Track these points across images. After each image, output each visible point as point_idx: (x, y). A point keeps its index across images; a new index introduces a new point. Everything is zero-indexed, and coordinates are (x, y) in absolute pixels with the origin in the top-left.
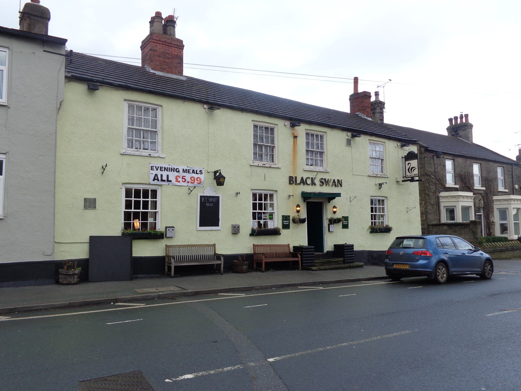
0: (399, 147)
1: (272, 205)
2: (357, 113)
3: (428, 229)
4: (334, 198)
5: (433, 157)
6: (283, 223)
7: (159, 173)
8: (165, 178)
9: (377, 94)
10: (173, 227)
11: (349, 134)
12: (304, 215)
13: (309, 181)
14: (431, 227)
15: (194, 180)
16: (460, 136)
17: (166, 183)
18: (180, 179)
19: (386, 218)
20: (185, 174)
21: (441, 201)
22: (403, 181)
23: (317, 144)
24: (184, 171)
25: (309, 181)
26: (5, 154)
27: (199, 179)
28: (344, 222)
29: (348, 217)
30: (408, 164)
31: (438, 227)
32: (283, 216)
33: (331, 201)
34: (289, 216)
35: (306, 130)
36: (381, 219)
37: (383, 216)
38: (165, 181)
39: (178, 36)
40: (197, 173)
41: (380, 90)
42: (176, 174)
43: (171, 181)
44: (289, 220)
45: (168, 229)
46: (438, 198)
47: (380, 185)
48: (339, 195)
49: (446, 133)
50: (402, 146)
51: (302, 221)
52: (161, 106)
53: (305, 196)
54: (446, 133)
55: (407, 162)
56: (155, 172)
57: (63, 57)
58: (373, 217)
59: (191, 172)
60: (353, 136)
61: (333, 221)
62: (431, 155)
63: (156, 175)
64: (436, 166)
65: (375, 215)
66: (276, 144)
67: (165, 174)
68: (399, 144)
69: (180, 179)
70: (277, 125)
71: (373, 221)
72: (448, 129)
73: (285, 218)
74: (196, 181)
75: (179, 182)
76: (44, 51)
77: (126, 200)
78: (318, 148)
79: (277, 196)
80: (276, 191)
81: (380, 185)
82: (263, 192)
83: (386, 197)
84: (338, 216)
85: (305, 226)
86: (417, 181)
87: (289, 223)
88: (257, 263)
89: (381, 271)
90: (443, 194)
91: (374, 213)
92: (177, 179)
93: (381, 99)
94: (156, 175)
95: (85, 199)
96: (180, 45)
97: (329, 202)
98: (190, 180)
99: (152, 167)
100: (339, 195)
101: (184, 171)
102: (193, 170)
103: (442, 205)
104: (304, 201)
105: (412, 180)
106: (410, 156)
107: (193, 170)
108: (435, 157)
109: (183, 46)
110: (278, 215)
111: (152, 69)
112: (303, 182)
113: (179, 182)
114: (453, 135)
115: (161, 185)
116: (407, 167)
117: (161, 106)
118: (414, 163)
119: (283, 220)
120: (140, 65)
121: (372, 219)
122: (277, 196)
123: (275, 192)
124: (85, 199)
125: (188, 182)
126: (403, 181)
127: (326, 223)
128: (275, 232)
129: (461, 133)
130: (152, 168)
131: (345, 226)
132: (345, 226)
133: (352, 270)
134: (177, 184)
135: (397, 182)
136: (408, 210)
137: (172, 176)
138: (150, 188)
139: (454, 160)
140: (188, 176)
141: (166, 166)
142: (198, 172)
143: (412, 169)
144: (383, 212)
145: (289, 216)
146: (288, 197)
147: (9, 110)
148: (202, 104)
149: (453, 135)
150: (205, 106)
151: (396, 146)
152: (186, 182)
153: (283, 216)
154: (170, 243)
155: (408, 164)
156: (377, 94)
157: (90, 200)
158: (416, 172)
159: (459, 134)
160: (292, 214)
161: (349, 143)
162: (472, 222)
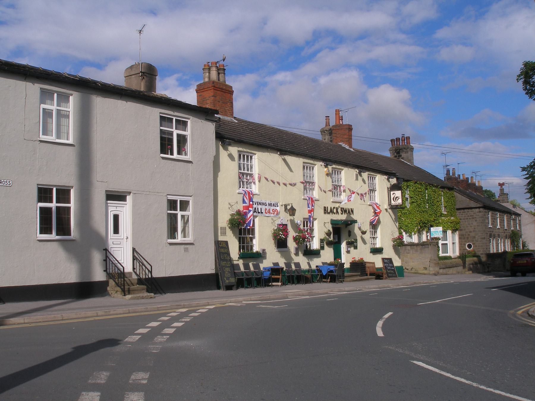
13: (335, 211)
16: (403, 158)
17: (260, 215)
23: (247, 165)
24: (270, 205)
25: (335, 211)
35: (304, 163)
55: (392, 193)
67: (260, 207)
73: (322, 241)
78: (248, 170)
88: (272, 274)
89: (374, 277)
101: (270, 205)
109: (233, 92)
112: (332, 211)
114: (396, 157)
116: (392, 197)
129: (403, 155)
131: (184, 205)
137: (264, 207)
143: (396, 198)
147: (302, 180)
149: (396, 157)
159: (401, 156)
162: (424, 242)
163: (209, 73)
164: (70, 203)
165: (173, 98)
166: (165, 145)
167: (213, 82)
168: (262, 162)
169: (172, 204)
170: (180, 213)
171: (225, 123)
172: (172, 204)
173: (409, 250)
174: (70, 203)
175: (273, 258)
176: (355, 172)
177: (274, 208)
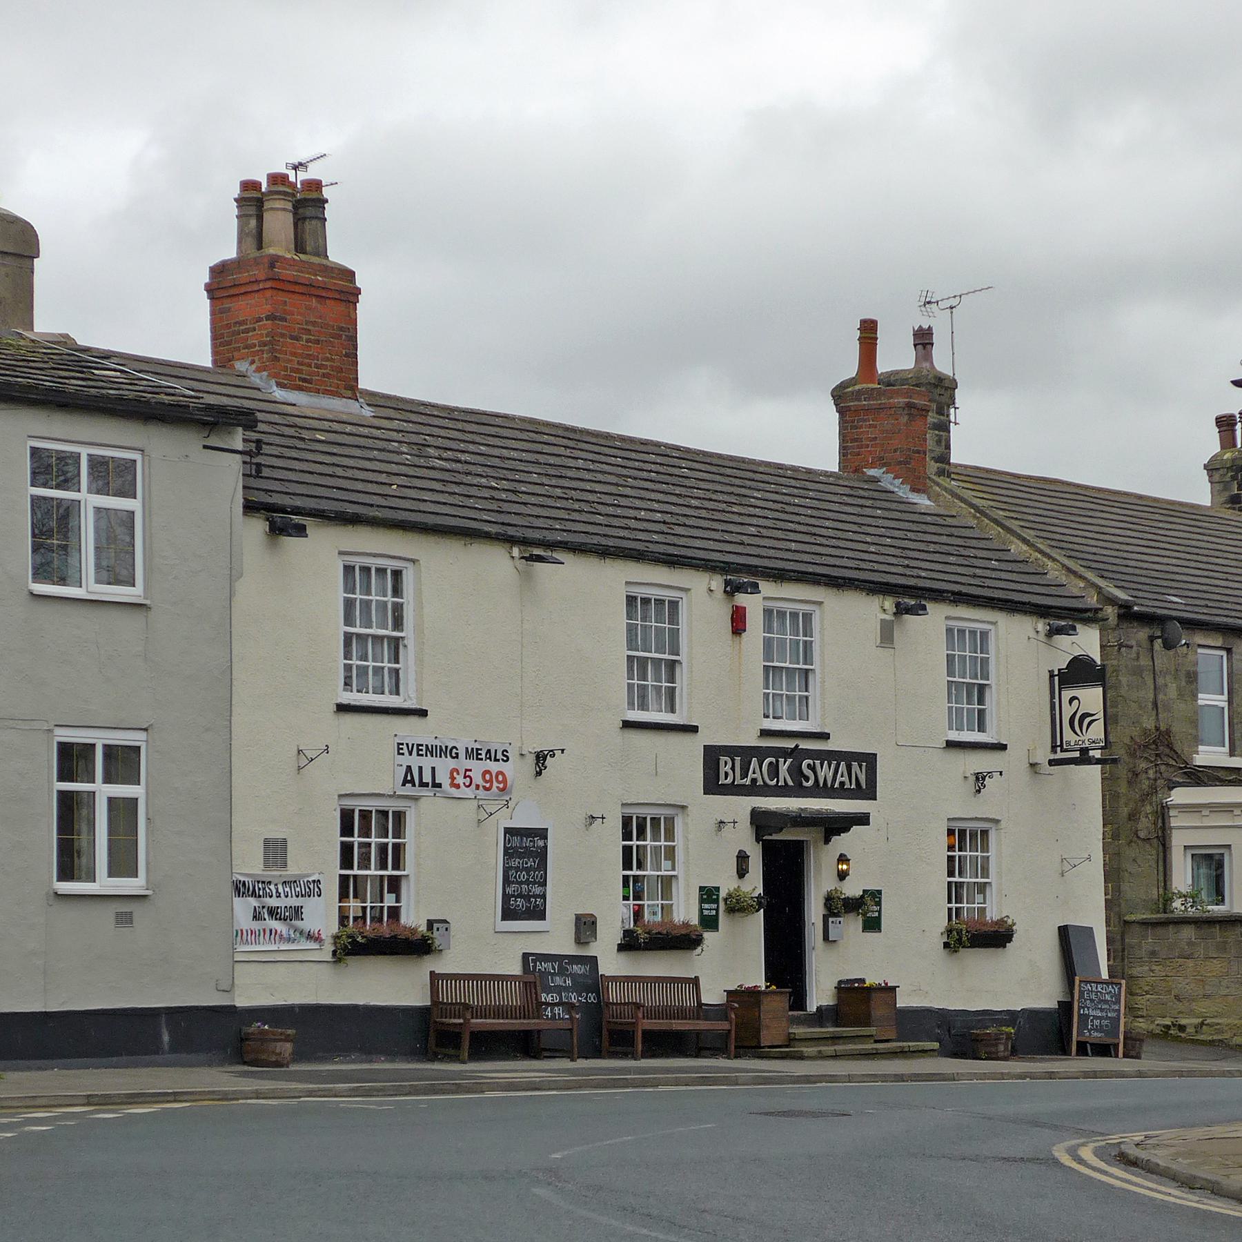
0: (1042, 637)
1: (671, 853)
2: (872, 472)
3: (1123, 939)
4: (847, 830)
5: (1152, 639)
6: (701, 910)
7: (414, 761)
8: (427, 778)
9: (923, 339)
10: (445, 921)
11: (889, 603)
12: (754, 884)
14: (1137, 929)
15: (491, 781)
18: (460, 780)
19: (992, 893)
20: (472, 764)
21: (1174, 823)
22: (1052, 763)
24: (473, 754)
26: (146, 730)
27: (500, 778)
28: (865, 909)
29: (879, 892)
30: (1071, 701)
31: (1160, 931)
32: (701, 889)
33: (834, 838)
34: (718, 889)
36: (979, 898)
37: (982, 888)
38: (427, 785)
39: (337, 253)
40: (496, 760)
41: (939, 325)
42: (451, 763)
43: (440, 786)
44: (716, 901)
45: (435, 926)
46: (1163, 813)
47: (980, 778)
48: (863, 819)
49: (1200, 493)
50: (1053, 632)
51: (737, 907)
52: (413, 561)
53: (761, 822)
54: (1200, 493)
55: (1067, 694)
56: (406, 760)
57: (238, 456)
58: (955, 892)
59: (483, 756)
60: (901, 610)
61: (836, 906)
62: (1142, 634)
63: (409, 768)
64: (1160, 681)
65: (959, 885)
66: (683, 657)
67: (427, 762)
68: (1041, 626)
69: (460, 780)
70: (687, 590)
71: (953, 905)
72: (1211, 468)
73: (708, 894)
74: (495, 784)
75: (458, 786)
76: (205, 447)
77: (342, 843)
79: (686, 824)
80: (683, 807)
81: (980, 778)
82: (649, 812)
83: (997, 821)
84: (852, 889)
85: (756, 922)
86: (1098, 762)
87: (717, 910)
90: (1180, 796)
91: (635, 872)
92: (453, 778)
93: (941, 362)
94: (409, 768)
95: (266, 841)
96: (343, 290)
97: (827, 841)
98: (481, 782)
99: (399, 744)
100: (863, 819)
101: (473, 754)
102: (489, 751)
103: (1178, 840)
104: (758, 840)
105: (1084, 758)
106: (1079, 672)
107: (489, 751)
108: (1158, 644)
110: (688, 885)
111: (280, 385)
113: (458, 786)
115: (416, 799)
117: (413, 561)
118: (1091, 698)
119: (702, 901)
120: (204, 358)
121: (950, 901)
122: (686, 824)
123: (680, 811)
124: (266, 841)
125: (478, 787)
126: (1052, 763)
127: (814, 911)
128: (685, 941)
130: (399, 749)
131: (873, 925)
132: (873, 925)
133: (906, 1058)
134: (454, 792)
135: (1032, 765)
136: (1067, 867)
137: (444, 766)
138: (391, 806)
139: (1229, 651)
140: (477, 768)
141: (430, 741)
142: (499, 756)
143: (1081, 720)
144: (985, 873)
145: (718, 889)
146: (714, 827)
148: (508, 545)
150: (516, 551)
151: (1032, 634)
152: (473, 786)
153: (701, 889)
154: (447, 964)
155: (1071, 701)
156: (923, 339)
157: (275, 841)
158: (1096, 731)
160: (727, 883)
161: (887, 636)
163: (260, 218)
164: (111, 874)
165: (82, 341)
166: (52, 534)
167: (274, 261)
168: (455, 588)
169: (72, 759)
170: (103, 791)
171: (297, 429)
172: (72, 759)
173: (1190, 944)
174: (111, 874)
175: (484, 948)
176: (497, 564)
177: (494, 767)
